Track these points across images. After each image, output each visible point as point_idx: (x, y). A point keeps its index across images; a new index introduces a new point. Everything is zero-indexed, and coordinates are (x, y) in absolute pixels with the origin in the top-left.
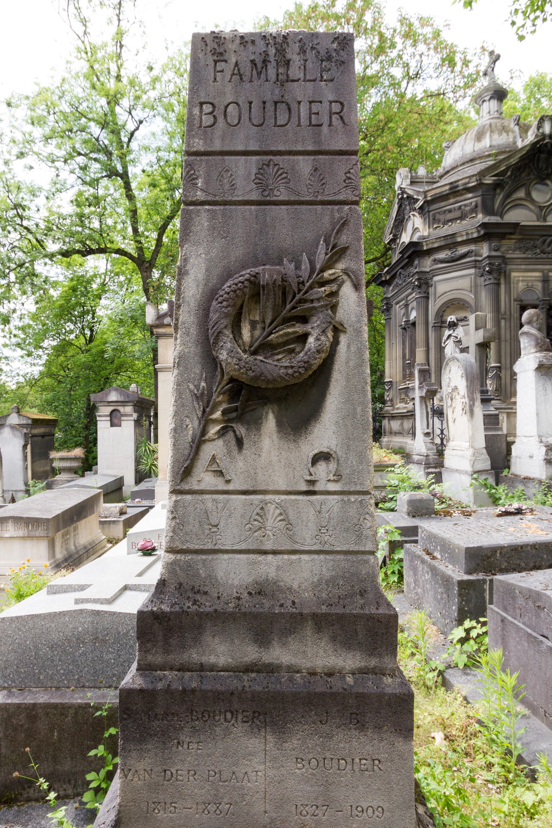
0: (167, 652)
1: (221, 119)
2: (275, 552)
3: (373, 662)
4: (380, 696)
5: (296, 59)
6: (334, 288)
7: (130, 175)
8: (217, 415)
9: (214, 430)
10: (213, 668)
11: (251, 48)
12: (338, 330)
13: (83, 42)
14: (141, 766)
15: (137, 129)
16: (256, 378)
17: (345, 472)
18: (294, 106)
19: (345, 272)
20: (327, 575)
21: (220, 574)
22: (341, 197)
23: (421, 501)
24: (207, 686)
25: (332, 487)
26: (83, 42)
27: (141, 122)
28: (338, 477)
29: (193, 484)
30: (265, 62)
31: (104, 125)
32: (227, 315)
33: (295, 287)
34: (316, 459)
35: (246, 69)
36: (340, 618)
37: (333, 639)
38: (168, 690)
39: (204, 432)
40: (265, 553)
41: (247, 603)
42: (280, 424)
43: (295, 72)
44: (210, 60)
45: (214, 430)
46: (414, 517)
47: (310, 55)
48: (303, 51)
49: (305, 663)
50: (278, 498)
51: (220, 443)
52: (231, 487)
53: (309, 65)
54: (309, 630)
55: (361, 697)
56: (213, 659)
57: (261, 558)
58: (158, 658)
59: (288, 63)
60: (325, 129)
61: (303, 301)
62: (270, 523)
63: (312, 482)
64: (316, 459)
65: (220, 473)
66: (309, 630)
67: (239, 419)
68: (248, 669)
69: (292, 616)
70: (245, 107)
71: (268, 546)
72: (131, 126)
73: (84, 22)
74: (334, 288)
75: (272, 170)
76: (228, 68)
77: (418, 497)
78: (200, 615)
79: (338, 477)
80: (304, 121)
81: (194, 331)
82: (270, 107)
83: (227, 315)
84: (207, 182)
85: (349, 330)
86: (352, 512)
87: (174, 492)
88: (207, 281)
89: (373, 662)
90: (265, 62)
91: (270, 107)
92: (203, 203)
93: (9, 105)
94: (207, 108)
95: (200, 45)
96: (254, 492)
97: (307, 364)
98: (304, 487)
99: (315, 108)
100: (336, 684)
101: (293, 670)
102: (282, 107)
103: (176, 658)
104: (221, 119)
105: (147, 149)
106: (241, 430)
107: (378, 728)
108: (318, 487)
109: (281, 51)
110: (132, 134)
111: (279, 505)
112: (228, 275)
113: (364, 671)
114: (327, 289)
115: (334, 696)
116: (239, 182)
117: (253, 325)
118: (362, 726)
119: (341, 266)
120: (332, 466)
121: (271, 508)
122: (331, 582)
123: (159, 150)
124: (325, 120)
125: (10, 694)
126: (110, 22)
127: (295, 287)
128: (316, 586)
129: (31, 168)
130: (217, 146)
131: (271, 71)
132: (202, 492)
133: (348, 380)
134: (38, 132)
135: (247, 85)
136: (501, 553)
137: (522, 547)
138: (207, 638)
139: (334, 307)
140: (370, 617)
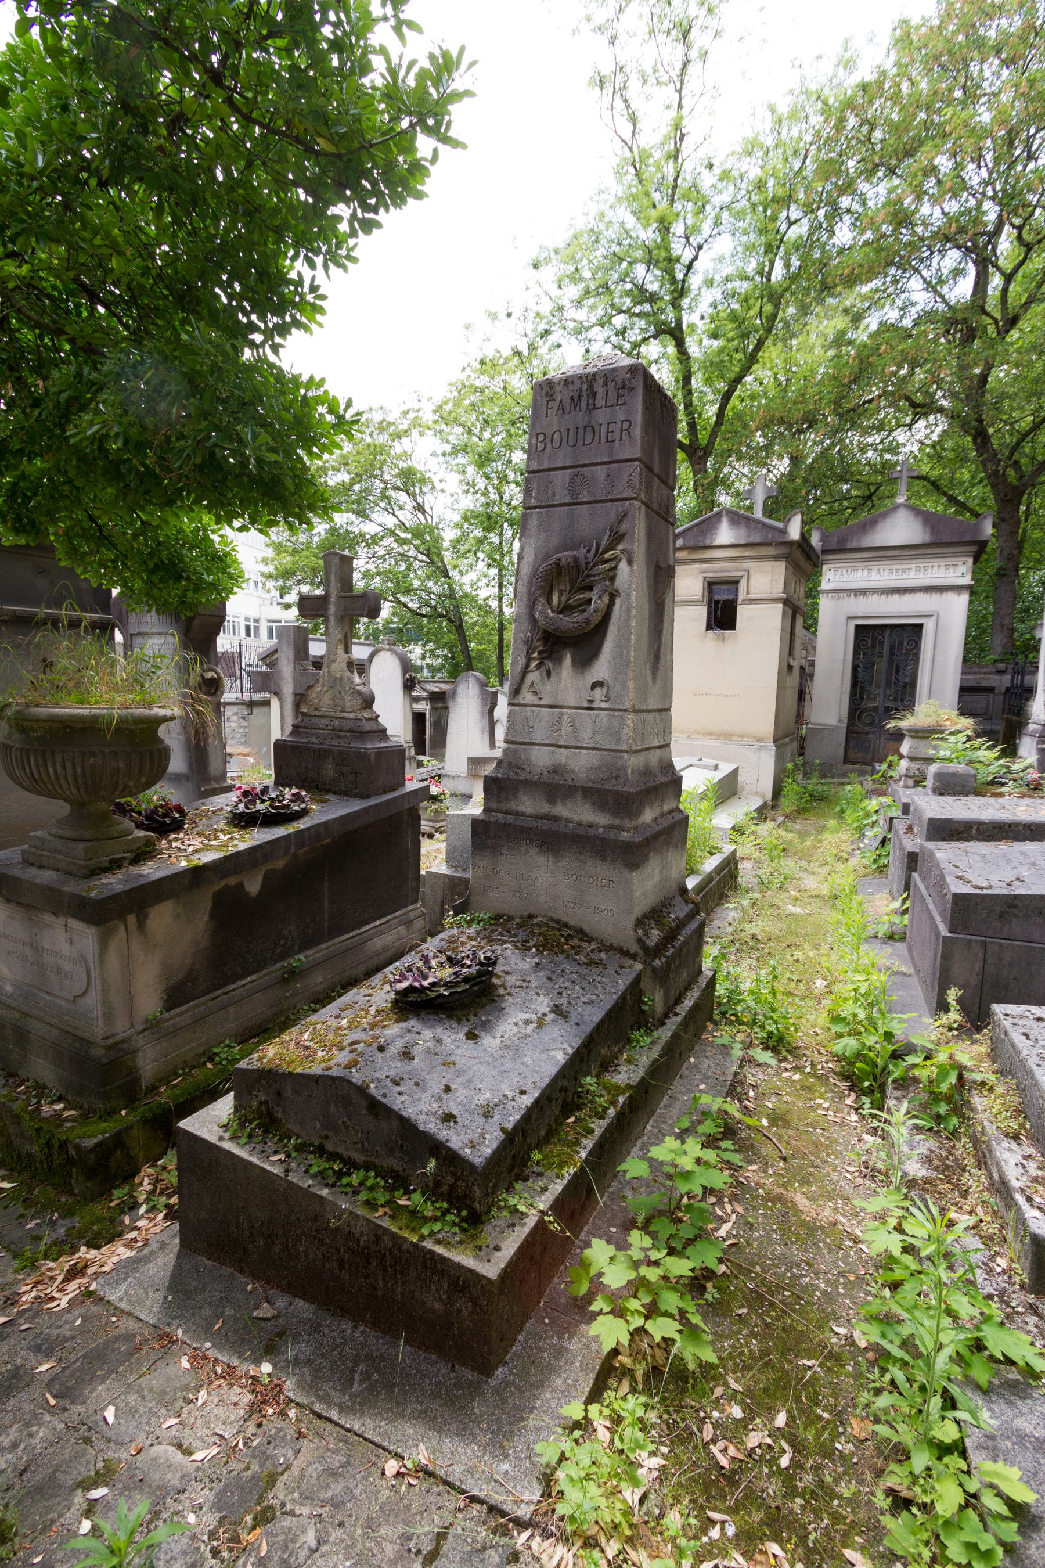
0: (499, 802)
1: (549, 445)
2: (566, 747)
3: (617, 822)
4: (616, 841)
5: (599, 389)
6: (613, 564)
7: (684, 327)
8: (535, 655)
9: (534, 664)
10: (523, 814)
11: (571, 387)
12: (613, 597)
13: (630, 149)
14: (482, 864)
15: (696, 258)
16: (556, 630)
17: (613, 695)
18: (597, 428)
19: (622, 551)
20: (597, 764)
21: (533, 759)
22: (624, 495)
23: (955, 775)
24: (518, 823)
25: (604, 705)
26: (630, 149)
27: (700, 247)
28: (607, 699)
29: (520, 700)
30: (580, 397)
31: (650, 262)
32: (540, 588)
33: (583, 565)
34: (595, 685)
35: (567, 404)
36: (599, 790)
37: (593, 804)
38: (496, 823)
39: (527, 666)
40: (560, 747)
41: (545, 778)
42: (574, 662)
43: (600, 402)
44: (545, 399)
45: (534, 664)
46: (941, 794)
47: (611, 386)
48: (605, 384)
49: (576, 818)
50: (569, 711)
51: (537, 673)
52: (542, 703)
53: (610, 394)
54: (579, 797)
55: (604, 840)
56: (523, 809)
57: (557, 750)
58: (494, 806)
59: (595, 395)
60: (617, 444)
61: (589, 576)
62: (563, 728)
63: (591, 701)
64: (595, 685)
65: (535, 693)
66: (579, 797)
67: (549, 658)
68: (543, 817)
69: (570, 787)
70: (565, 433)
71: (562, 742)
72: (687, 255)
73: (633, 120)
74: (613, 564)
75: (579, 479)
76: (555, 405)
77: (951, 770)
78: (517, 781)
79: (607, 699)
80: (603, 439)
81: (525, 598)
82: (581, 431)
83: (540, 588)
84: (538, 493)
85: (623, 594)
86: (615, 723)
87: (510, 704)
88: (535, 562)
89: (617, 822)
90: (580, 397)
91: (581, 431)
92: (535, 508)
93: (536, 267)
94: (541, 438)
95: (538, 389)
96: (556, 707)
97: (588, 621)
98: (586, 705)
99: (612, 427)
100: (592, 832)
101: (568, 821)
102: (589, 430)
103: (503, 806)
104: (549, 445)
105: (710, 283)
106: (549, 664)
107: (614, 861)
108: (595, 705)
109: (591, 387)
110: (689, 267)
111: (570, 716)
112: (547, 557)
113: (610, 827)
114: (607, 566)
115: (588, 837)
116: (558, 490)
117: (561, 592)
118: (603, 859)
119: (620, 547)
120: (605, 691)
121: (565, 717)
122: (599, 769)
123: (728, 279)
124: (618, 437)
125: (456, 871)
126: (704, 55)
127: (583, 565)
128: (589, 770)
129: (559, 346)
130: (545, 466)
131: (584, 403)
132: (525, 705)
133: (619, 630)
134: (573, 291)
135: (567, 417)
136: (978, 829)
137: (1010, 825)
138: (521, 795)
139: (612, 579)
140: (617, 792)
